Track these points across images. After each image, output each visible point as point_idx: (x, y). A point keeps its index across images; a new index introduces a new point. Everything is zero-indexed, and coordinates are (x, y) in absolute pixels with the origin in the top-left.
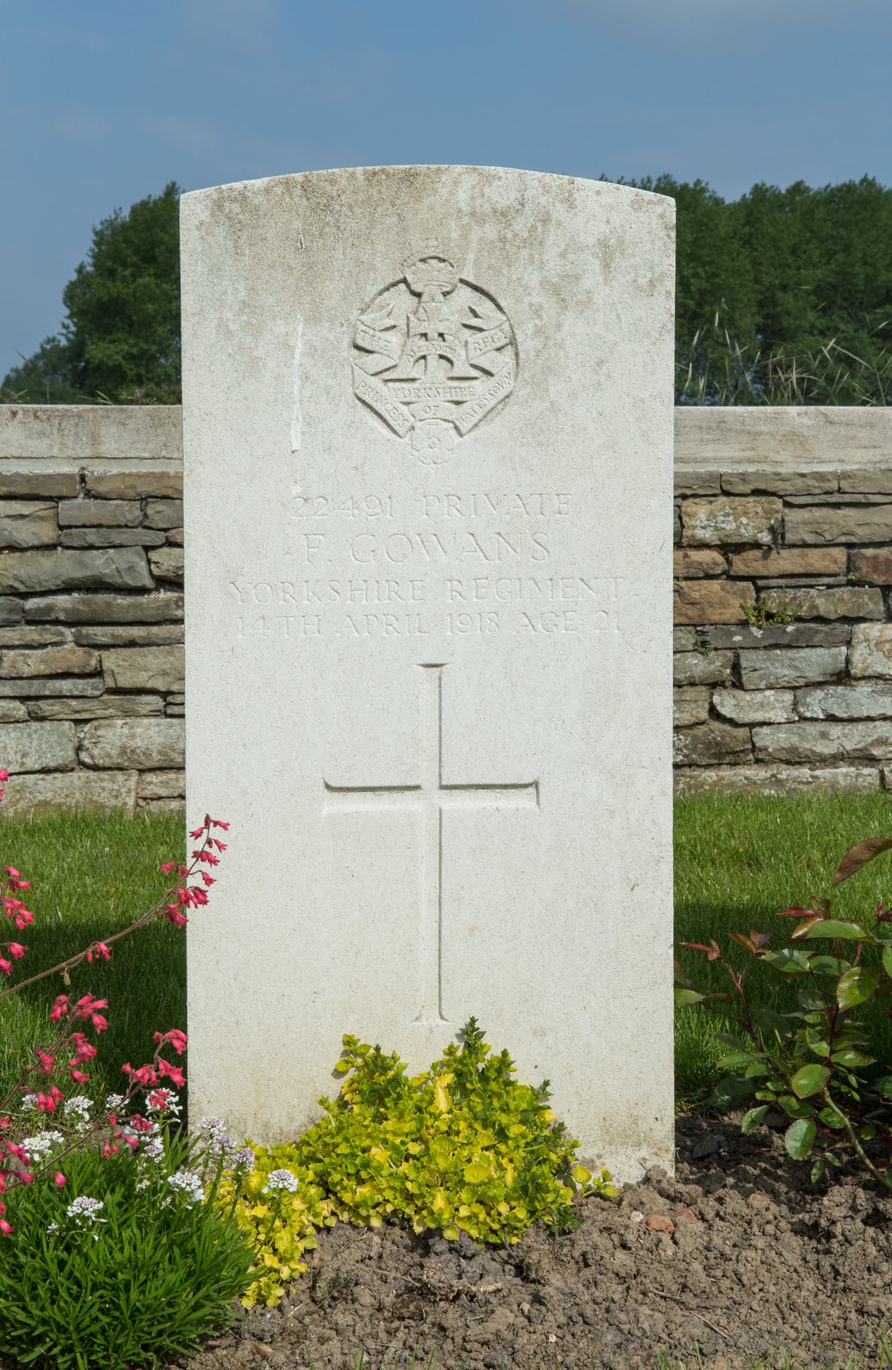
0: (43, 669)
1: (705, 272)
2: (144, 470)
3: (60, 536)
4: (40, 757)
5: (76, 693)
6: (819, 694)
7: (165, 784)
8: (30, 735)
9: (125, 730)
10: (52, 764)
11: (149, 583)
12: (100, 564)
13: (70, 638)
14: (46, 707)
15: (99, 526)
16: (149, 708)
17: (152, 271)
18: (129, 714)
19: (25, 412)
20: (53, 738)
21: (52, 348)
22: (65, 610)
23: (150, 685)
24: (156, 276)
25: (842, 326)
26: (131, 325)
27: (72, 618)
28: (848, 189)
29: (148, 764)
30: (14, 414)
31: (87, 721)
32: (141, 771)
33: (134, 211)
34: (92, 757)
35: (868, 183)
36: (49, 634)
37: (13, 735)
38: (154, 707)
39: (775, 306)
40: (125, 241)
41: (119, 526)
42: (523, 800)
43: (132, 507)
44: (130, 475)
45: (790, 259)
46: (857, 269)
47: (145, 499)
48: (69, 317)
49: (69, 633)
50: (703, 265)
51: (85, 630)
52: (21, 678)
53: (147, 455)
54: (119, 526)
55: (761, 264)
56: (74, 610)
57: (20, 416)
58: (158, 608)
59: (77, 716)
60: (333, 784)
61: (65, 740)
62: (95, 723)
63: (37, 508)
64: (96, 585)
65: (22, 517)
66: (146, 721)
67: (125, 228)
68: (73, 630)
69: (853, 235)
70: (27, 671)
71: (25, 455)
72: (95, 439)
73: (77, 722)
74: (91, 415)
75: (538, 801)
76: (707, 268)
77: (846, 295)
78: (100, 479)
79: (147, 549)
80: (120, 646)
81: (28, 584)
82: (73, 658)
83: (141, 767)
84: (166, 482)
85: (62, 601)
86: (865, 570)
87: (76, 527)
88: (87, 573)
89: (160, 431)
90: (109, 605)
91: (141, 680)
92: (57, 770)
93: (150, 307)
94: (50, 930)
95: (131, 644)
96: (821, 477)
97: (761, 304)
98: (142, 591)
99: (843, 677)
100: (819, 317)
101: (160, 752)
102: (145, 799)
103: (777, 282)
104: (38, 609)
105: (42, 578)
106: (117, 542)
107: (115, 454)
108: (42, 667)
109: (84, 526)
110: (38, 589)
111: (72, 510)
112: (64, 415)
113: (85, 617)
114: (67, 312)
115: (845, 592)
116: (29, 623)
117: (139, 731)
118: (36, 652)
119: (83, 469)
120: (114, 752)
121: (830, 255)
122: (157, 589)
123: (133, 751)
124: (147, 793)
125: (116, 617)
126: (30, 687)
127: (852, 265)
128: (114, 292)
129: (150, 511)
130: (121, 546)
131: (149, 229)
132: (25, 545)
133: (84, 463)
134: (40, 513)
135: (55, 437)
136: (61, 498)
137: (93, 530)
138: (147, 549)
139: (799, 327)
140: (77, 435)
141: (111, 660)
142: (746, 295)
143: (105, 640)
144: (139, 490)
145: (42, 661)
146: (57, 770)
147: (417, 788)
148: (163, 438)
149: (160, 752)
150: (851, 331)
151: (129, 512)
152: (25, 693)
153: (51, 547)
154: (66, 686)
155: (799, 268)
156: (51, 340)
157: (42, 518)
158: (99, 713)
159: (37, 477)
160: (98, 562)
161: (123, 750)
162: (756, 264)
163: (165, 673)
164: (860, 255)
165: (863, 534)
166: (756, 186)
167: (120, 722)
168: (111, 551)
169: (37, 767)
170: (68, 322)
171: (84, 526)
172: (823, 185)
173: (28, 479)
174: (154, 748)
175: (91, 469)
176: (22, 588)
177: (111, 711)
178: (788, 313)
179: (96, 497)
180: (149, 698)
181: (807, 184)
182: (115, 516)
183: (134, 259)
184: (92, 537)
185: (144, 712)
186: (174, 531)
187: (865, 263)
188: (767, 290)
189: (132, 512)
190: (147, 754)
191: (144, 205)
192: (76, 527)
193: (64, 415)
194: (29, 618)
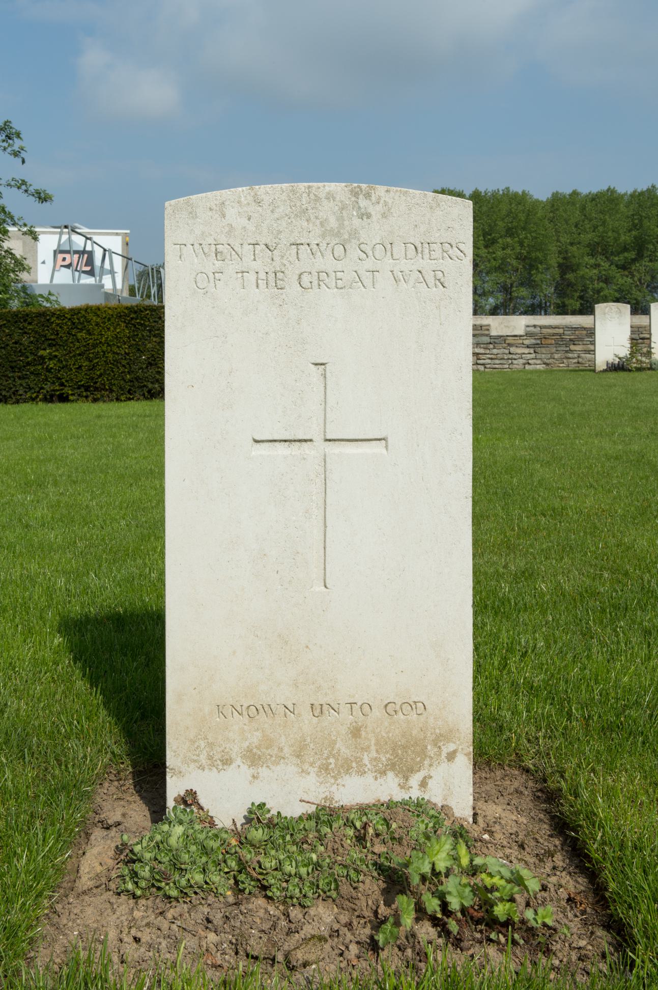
25: (602, 264)
35: (611, 191)
45: (574, 230)
55: (559, 232)
60: (257, 438)
69: (607, 217)
94: (81, 622)
97: (560, 253)
121: (595, 228)
147: (311, 440)
162: (557, 231)
164: (610, 227)
166: (553, 193)
172: (588, 192)
187: (613, 231)
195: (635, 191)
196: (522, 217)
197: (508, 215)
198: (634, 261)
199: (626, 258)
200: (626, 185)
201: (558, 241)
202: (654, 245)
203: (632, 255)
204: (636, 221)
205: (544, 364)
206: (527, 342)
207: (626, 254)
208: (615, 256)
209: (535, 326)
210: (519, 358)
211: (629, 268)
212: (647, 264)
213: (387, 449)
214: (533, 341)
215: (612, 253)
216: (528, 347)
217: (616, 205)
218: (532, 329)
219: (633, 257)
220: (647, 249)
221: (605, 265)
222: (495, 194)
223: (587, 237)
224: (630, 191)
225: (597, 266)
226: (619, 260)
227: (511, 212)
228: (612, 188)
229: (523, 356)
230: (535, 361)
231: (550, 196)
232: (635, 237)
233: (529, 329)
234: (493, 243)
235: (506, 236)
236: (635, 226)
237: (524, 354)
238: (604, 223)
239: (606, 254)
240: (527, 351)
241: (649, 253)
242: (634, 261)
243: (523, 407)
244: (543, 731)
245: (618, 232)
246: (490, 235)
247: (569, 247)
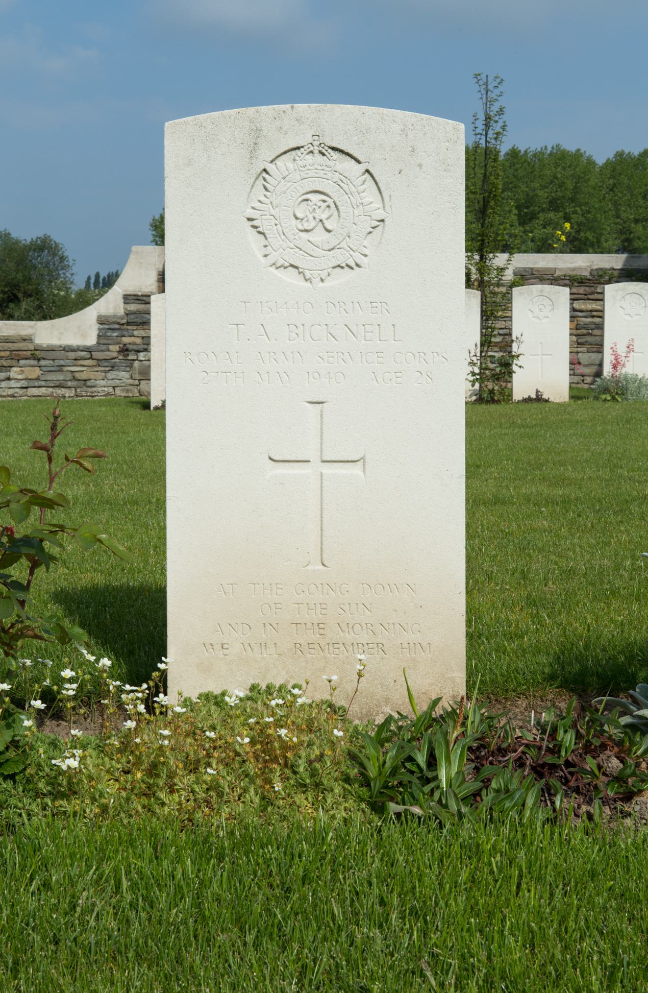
1: (581, 210)
6: (4, 382)
42: (355, 470)
45: (641, 202)
50: (580, 206)
75: (364, 470)
76: (583, 207)
86: (13, 356)
96: (3, 336)
99: (9, 379)
103: (632, 217)
115: (9, 361)
142: (608, 225)
147: (309, 461)
162: (616, 205)
165: (12, 348)
188: (624, 222)
196: (570, 184)
197: (551, 182)
201: (618, 217)
213: (321, 473)
222: (539, 155)
227: (555, 177)
231: (611, 156)
234: (531, 219)
235: (549, 210)
244: (555, 926)
246: (528, 207)
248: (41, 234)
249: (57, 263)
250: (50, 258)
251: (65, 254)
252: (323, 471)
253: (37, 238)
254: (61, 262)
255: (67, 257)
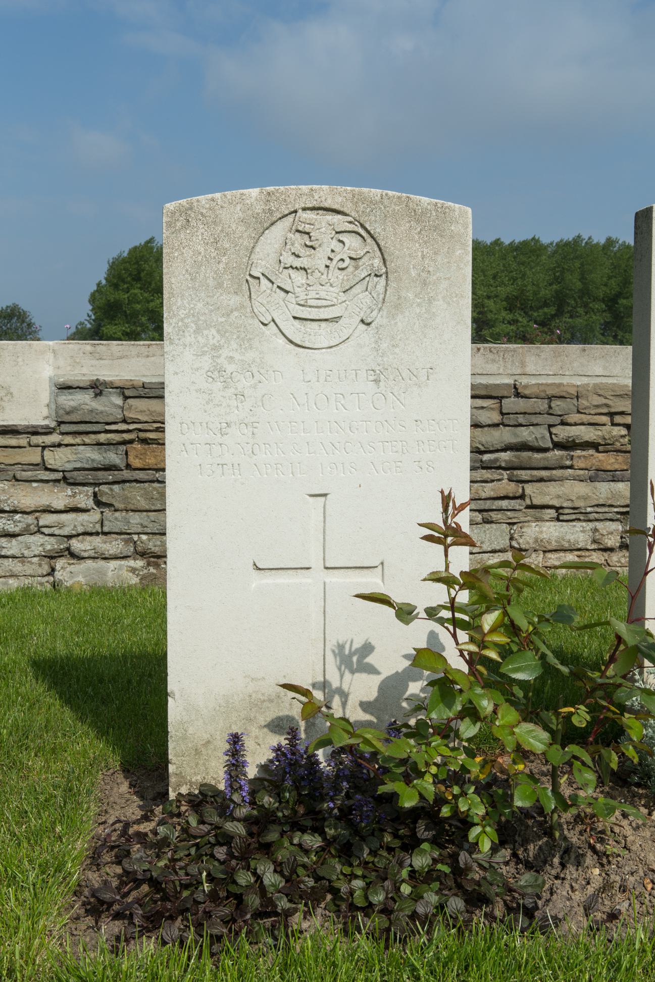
0: (492, 494)
2: (549, 382)
3: (502, 419)
4: (491, 544)
5: (510, 508)
7: (559, 559)
8: (485, 531)
9: (537, 529)
10: (498, 548)
11: (551, 445)
12: (525, 435)
13: (506, 477)
14: (494, 516)
15: (525, 413)
16: (549, 516)
17: (139, 285)
18: (538, 520)
19: (485, 348)
20: (498, 533)
21: (82, 328)
22: (505, 461)
23: (551, 503)
24: (141, 288)
25: (520, 319)
26: (126, 316)
27: (509, 465)
28: (525, 243)
29: (550, 548)
30: (479, 349)
31: (514, 524)
32: (544, 552)
33: (130, 252)
34: (519, 544)
36: (494, 474)
37: (475, 531)
38: (552, 516)
39: (483, 308)
40: (124, 269)
41: (536, 414)
43: (543, 402)
44: (542, 384)
45: (492, 282)
46: (529, 288)
47: (550, 398)
48: (92, 310)
49: (505, 474)
51: (515, 472)
52: (480, 499)
53: (551, 373)
54: (536, 414)
56: (510, 461)
57: (482, 350)
58: (557, 460)
59: (510, 521)
61: (504, 534)
62: (520, 525)
63: (490, 403)
64: (523, 447)
65: (483, 408)
66: (547, 523)
67: (124, 261)
68: (508, 472)
70: (484, 495)
71: (484, 373)
72: (523, 364)
73: (509, 524)
74: (521, 350)
77: (523, 301)
78: (526, 387)
79: (550, 426)
80: (534, 481)
81: (486, 446)
82: (510, 488)
83: (545, 549)
84: (562, 388)
85: (505, 456)
87: (512, 414)
88: (519, 440)
89: (559, 359)
90: (530, 458)
91: (547, 500)
92: (500, 551)
93: (138, 307)
95: (541, 480)
98: (546, 450)
100: (508, 314)
101: (556, 541)
102: (546, 567)
103: (485, 294)
104: (490, 461)
105: (494, 442)
106: (535, 422)
107: (534, 372)
108: (492, 493)
109: (516, 413)
110: (491, 449)
111: (510, 404)
112: (506, 350)
113: (516, 465)
114: (91, 307)
116: (483, 468)
117: (545, 529)
118: (488, 484)
119: (516, 381)
120: (531, 541)
121: (515, 280)
122: (553, 450)
123: (541, 541)
124: (548, 564)
125: (523, 465)
126: (485, 504)
127: (526, 286)
128: (117, 297)
129: (553, 405)
130: (537, 425)
131: (137, 263)
132: (484, 424)
133: (517, 377)
134: (492, 406)
135: (501, 362)
136: (503, 397)
137: (522, 415)
138: (550, 426)
139: (497, 319)
140: (513, 361)
141: (529, 489)
143: (527, 478)
144: (547, 393)
145: (492, 490)
146: (500, 551)
148: (560, 364)
149: (556, 541)
150: (525, 322)
151: (542, 405)
152: (482, 507)
153: (496, 425)
154: (504, 504)
155: (496, 287)
156: (81, 324)
157: (492, 409)
158: (522, 519)
159: (491, 385)
160: (524, 434)
161: (536, 540)
163: (559, 497)
167: (534, 524)
168: (531, 427)
169: (489, 549)
170: (90, 313)
171: (516, 413)
173: (486, 386)
174: (553, 539)
175: (520, 381)
176: (482, 449)
177: (529, 518)
178: (491, 312)
179: (522, 397)
180: (549, 511)
181: (502, 240)
182: (534, 407)
183: (129, 279)
184: (521, 419)
185: (547, 519)
186: (566, 416)
189: (543, 405)
190: (549, 542)
191: (135, 248)
192: (512, 414)
193: (506, 350)
194: (484, 465)
195: (561, 241)
198: (553, 317)
199: (545, 314)
200: (550, 236)
202: (575, 300)
203: (551, 310)
204: (557, 274)
205: (143, 554)
206: (58, 459)
207: (546, 310)
208: (535, 311)
209: (97, 388)
210: (26, 531)
211: (548, 324)
212: (567, 320)
214: (94, 456)
215: (532, 308)
216: (66, 480)
217: (538, 256)
218: (84, 399)
219: (553, 313)
220: (568, 304)
221: (523, 320)
223: (503, 291)
224: (556, 240)
225: (515, 322)
226: (539, 316)
228: (537, 238)
229: (47, 519)
230: (97, 541)
232: (556, 292)
233: (70, 400)
236: (556, 278)
237: (48, 510)
238: (524, 276)
239: (525, 309)
240: (60, 497)
241: (570, 309)
242: (553, 317)
243: (30, 763)
245: (538, 285)
247: (486, 301)
248: (10, 303)
249: (25, 329)
250: (18, 324)
251: (32, 321)
252: (327, 580)
253: (7, 307)
254: (28, 328)
255: (34, 324)
